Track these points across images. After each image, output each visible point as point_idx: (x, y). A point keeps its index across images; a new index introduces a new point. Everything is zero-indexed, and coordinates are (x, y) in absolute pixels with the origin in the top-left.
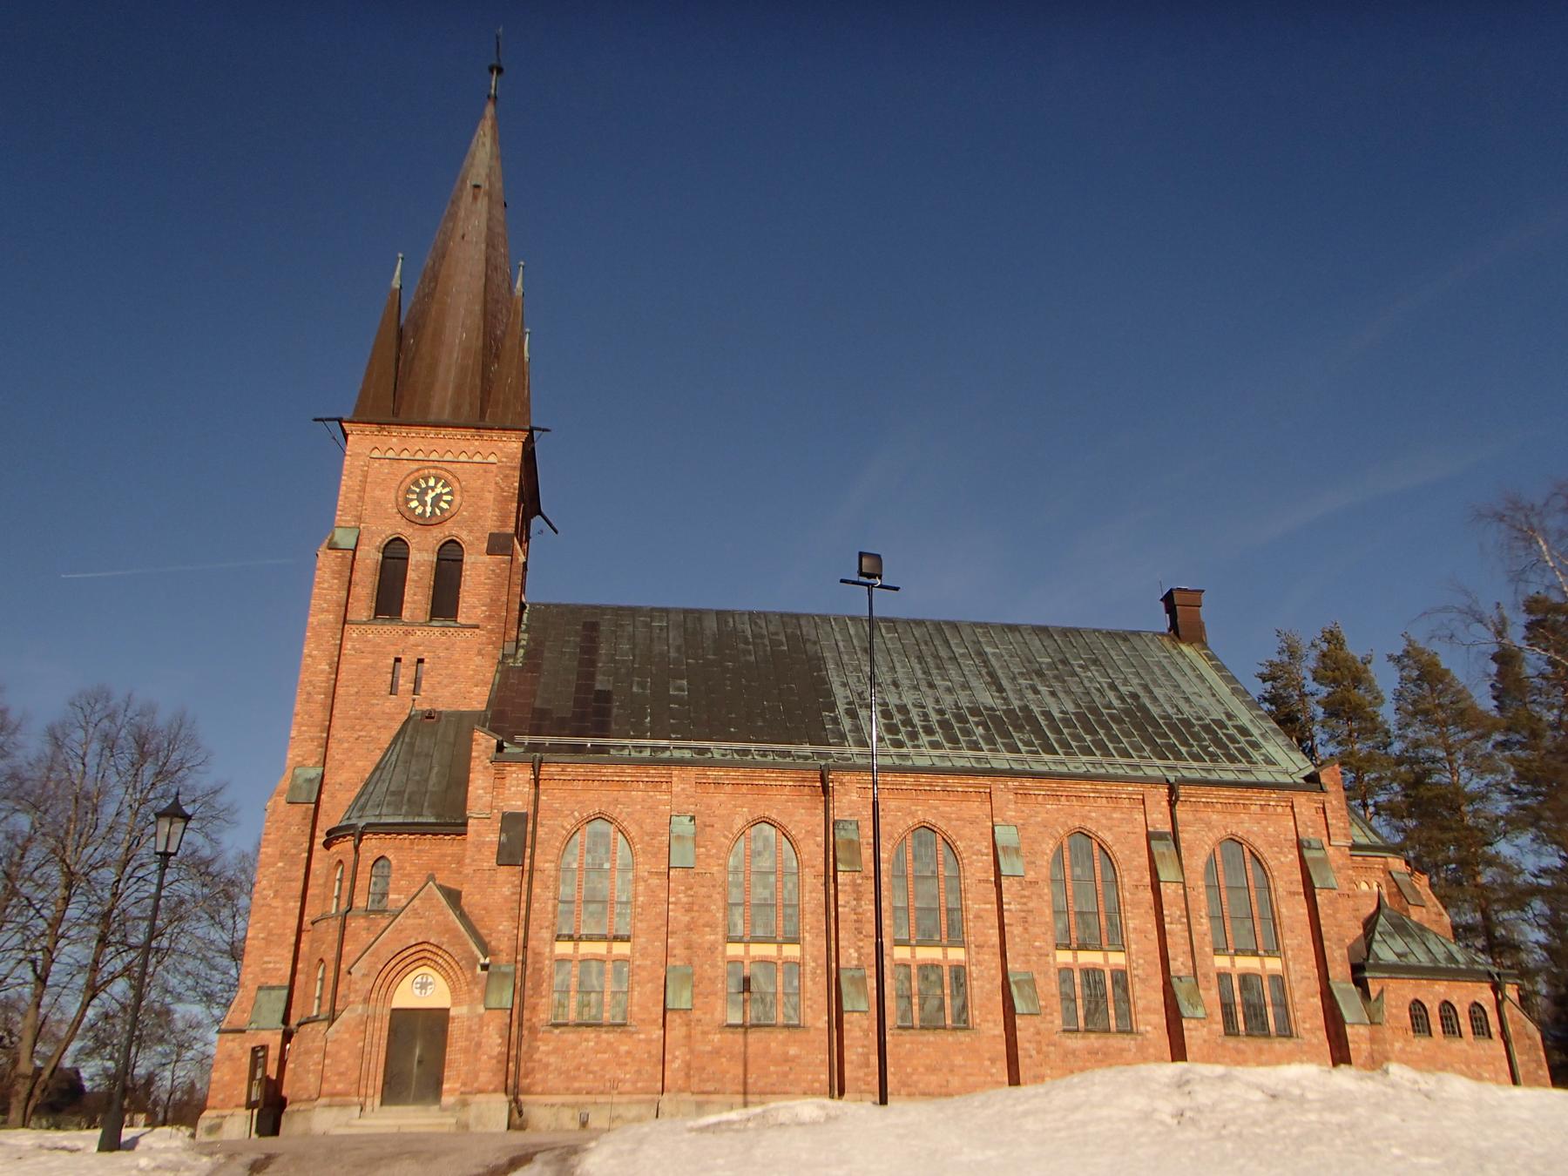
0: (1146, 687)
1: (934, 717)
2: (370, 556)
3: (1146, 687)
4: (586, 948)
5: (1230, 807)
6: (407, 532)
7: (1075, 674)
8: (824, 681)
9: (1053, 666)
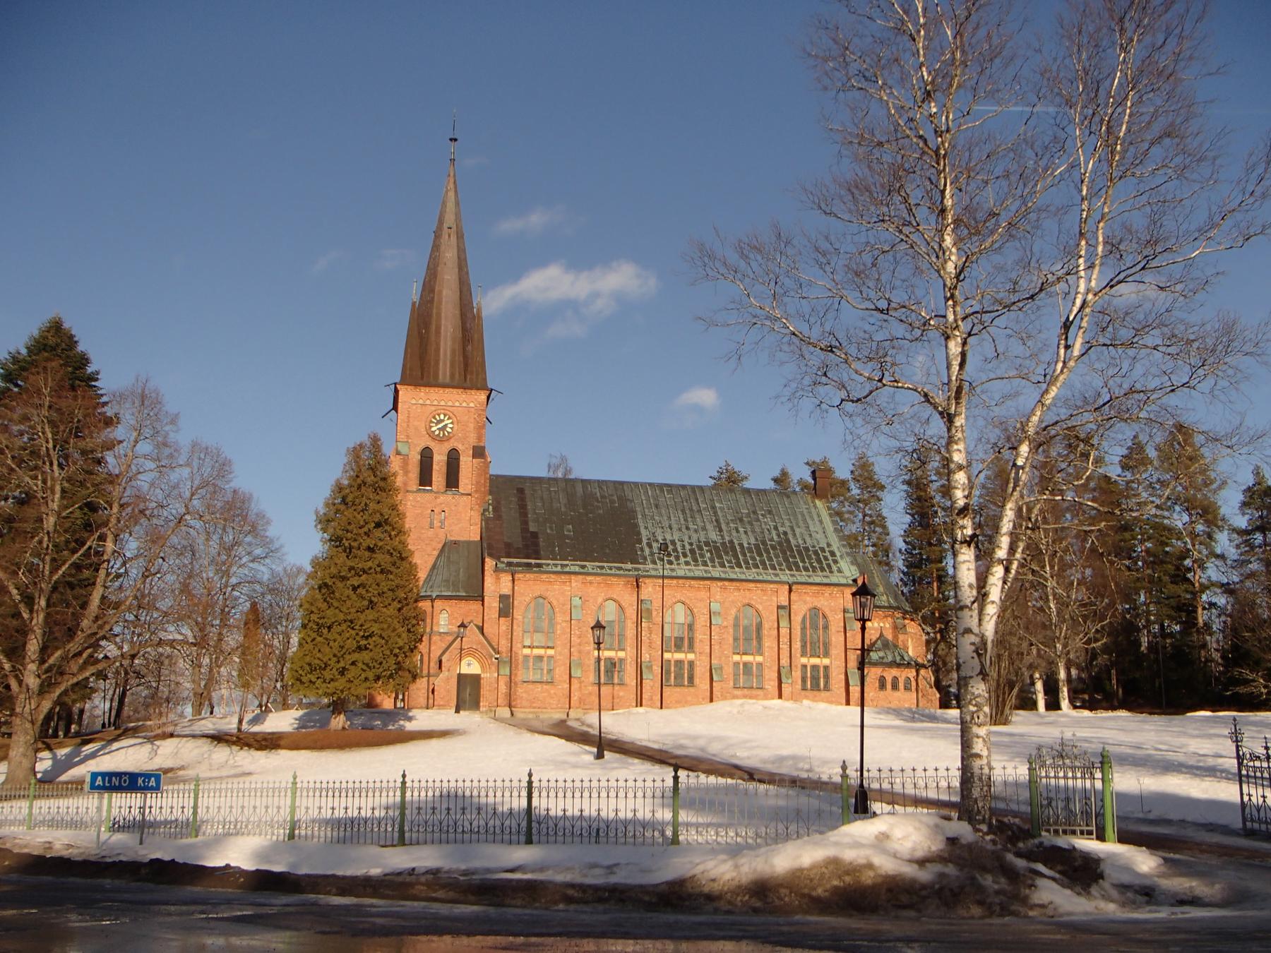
0: (792, 528)
1: (688, 547)
2: (415, 457)
3: (792, 528)
4: (536, 652)
5: (816, 595)
6: (432, 444)
7: (758, 520)
8: (636, 526)
9: (748, 515)
